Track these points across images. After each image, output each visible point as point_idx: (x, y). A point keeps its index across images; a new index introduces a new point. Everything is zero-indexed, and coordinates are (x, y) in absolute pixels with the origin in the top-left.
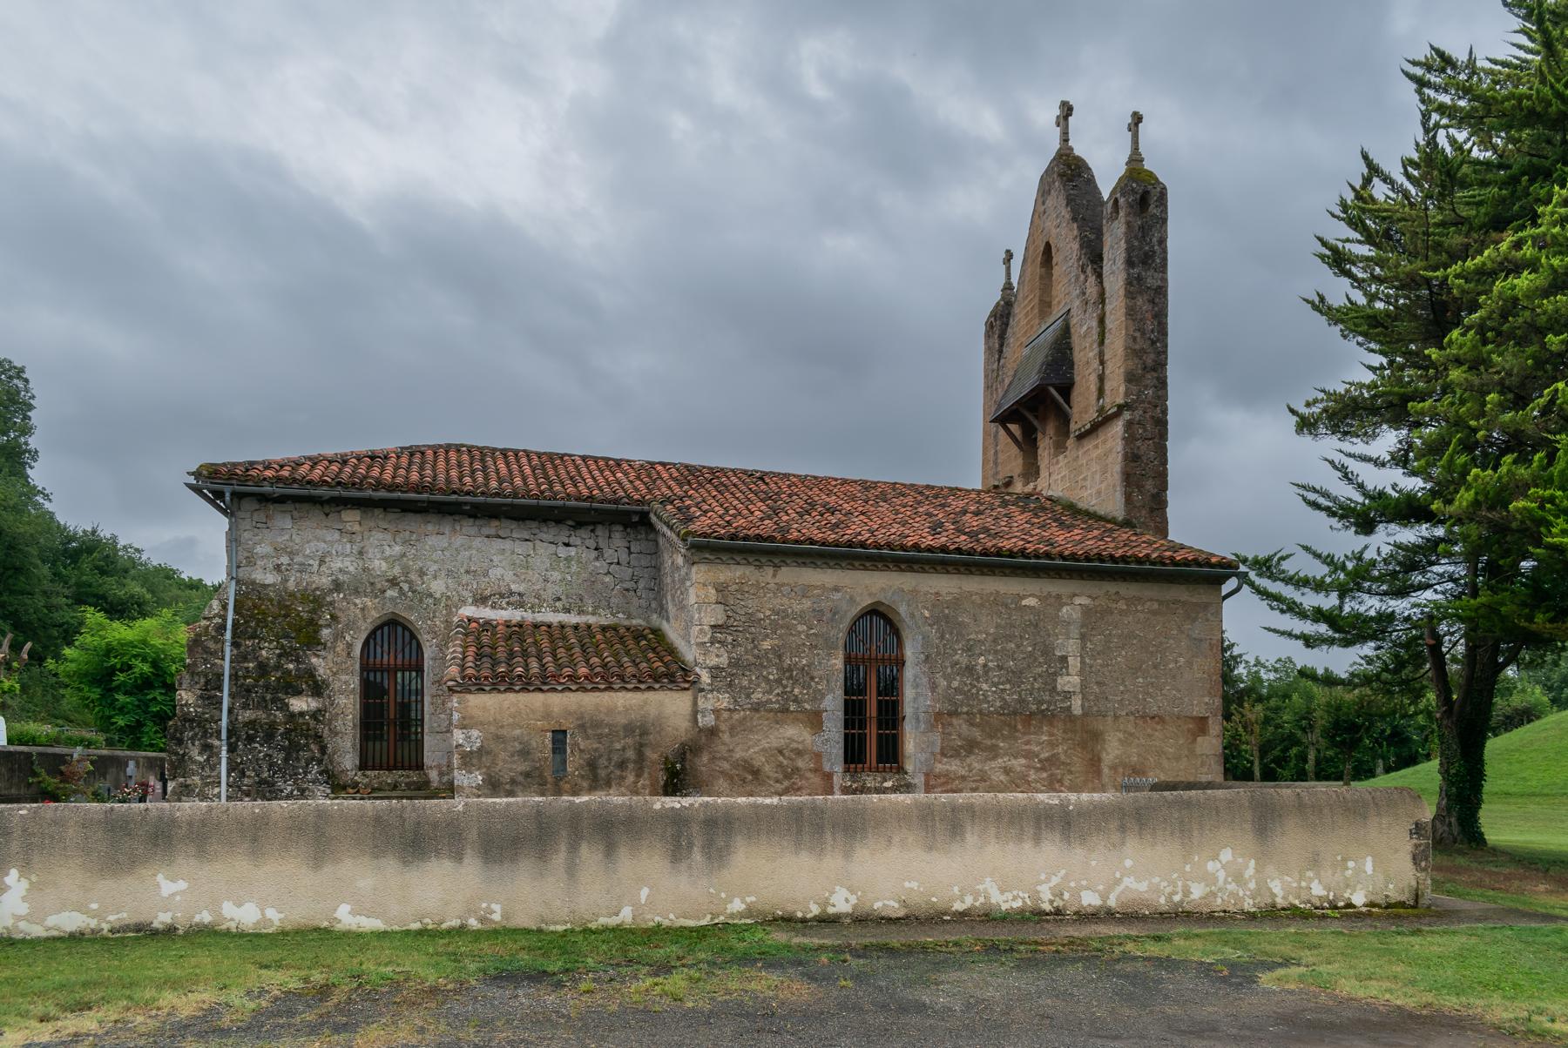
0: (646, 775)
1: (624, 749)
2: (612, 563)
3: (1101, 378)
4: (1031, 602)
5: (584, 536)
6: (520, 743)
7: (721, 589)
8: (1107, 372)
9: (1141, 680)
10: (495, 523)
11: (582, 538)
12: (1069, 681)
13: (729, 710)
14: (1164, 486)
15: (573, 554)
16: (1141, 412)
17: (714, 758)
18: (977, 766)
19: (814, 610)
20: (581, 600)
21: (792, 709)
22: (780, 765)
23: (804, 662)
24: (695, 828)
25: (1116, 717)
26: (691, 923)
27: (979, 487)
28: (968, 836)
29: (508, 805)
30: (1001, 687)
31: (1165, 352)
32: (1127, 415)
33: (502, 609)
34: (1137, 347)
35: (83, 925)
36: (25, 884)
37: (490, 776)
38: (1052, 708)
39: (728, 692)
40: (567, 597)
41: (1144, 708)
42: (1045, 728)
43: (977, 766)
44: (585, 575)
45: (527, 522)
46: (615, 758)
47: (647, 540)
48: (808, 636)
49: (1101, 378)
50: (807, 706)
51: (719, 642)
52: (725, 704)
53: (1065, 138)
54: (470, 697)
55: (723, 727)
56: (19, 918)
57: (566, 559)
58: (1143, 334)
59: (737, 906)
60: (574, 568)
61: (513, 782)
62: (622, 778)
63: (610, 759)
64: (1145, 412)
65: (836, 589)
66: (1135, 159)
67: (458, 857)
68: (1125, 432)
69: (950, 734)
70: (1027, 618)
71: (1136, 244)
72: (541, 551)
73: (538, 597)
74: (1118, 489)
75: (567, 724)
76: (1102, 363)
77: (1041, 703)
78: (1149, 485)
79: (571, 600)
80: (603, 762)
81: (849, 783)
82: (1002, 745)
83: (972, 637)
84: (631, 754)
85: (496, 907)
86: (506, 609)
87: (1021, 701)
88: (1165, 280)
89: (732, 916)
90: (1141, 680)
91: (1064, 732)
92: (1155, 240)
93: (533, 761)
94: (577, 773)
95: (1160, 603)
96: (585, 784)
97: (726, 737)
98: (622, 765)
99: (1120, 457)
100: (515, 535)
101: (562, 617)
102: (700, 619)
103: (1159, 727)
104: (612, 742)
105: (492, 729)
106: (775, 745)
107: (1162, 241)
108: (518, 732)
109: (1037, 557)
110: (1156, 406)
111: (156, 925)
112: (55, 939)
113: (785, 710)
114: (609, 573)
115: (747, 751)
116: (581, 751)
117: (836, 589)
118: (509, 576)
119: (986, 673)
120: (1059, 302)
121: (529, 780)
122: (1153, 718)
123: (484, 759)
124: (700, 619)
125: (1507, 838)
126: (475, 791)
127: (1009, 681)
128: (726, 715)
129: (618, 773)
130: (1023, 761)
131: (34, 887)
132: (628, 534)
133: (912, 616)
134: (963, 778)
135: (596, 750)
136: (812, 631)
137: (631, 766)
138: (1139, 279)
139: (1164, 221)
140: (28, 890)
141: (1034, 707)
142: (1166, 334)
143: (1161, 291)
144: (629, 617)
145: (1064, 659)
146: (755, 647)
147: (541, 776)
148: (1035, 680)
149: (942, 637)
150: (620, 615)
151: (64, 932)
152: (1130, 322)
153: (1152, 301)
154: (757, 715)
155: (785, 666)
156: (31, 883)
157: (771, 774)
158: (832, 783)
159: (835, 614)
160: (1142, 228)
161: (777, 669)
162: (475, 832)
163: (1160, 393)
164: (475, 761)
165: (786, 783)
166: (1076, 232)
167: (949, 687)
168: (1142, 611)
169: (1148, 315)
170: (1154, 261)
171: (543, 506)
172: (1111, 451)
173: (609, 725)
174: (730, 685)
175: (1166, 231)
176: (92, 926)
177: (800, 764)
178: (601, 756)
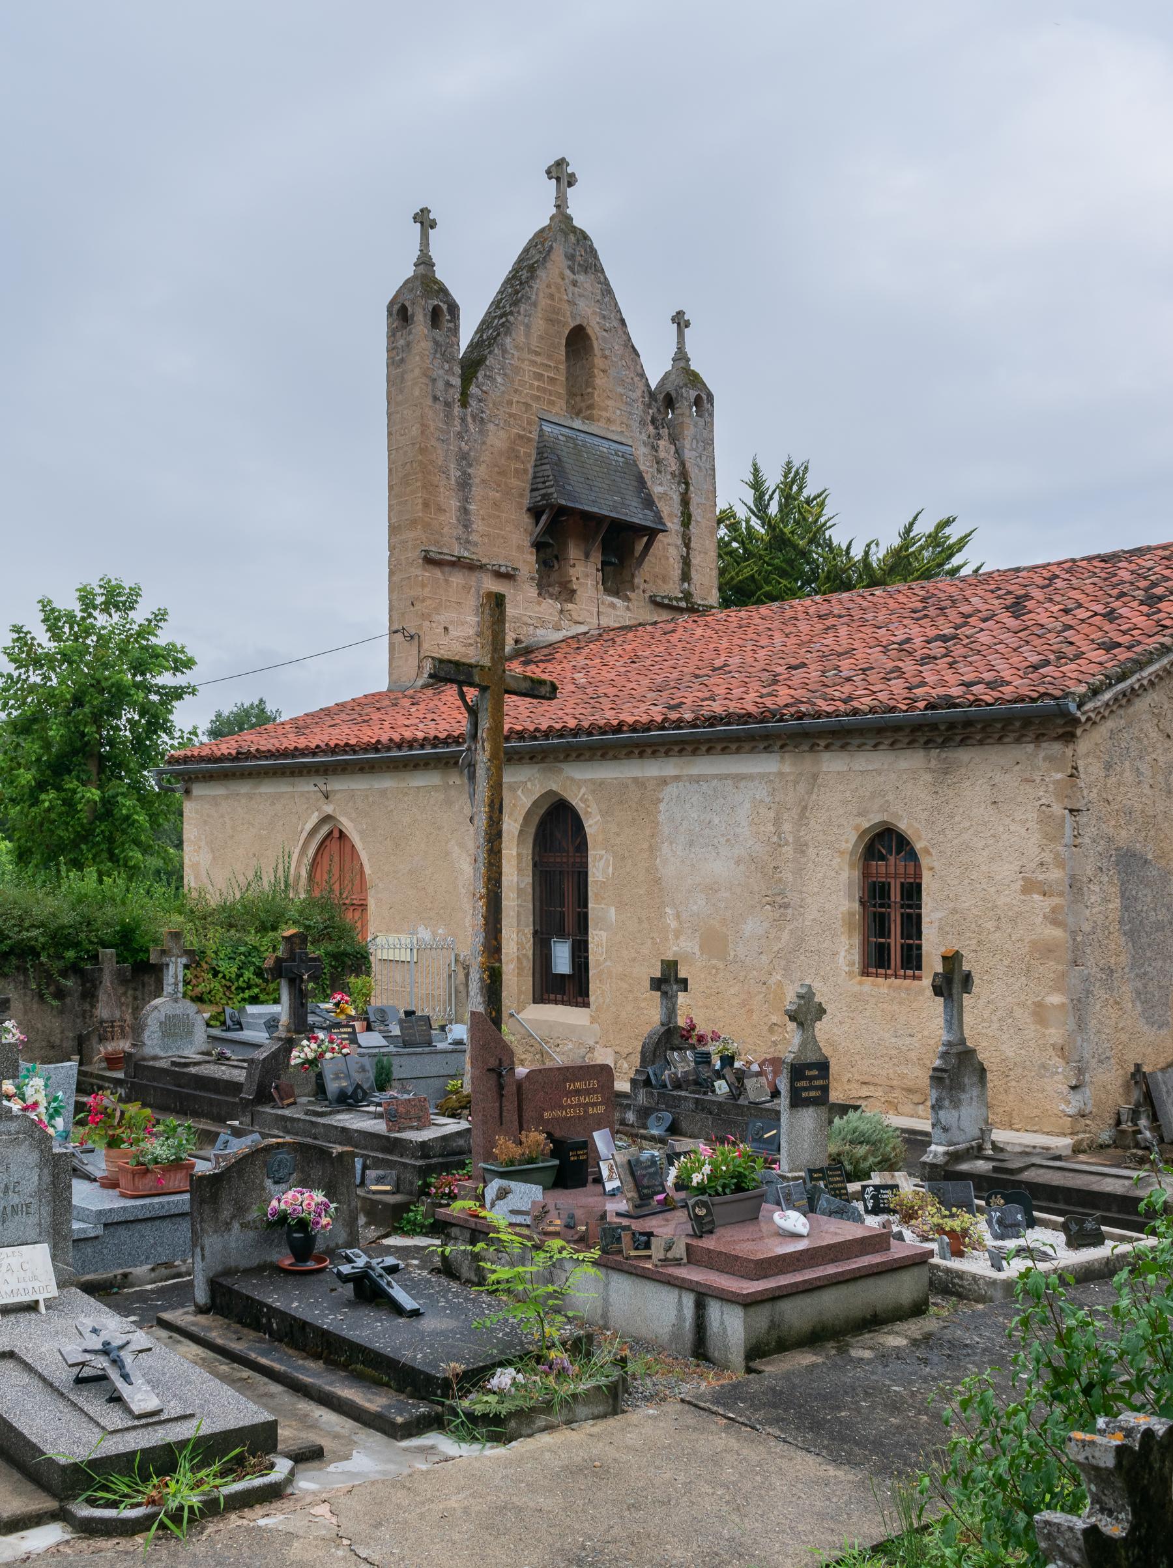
3: (686, 562)
49: (686, 562)
66: (425, 262)
76: (687, 545)
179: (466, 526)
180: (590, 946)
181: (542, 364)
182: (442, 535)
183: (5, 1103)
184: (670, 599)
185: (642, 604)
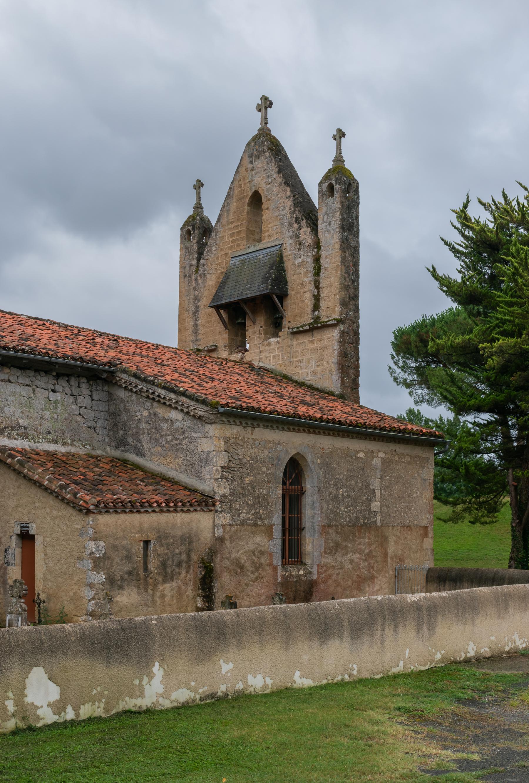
0: (191, 571)
1: (180, 553)
2: (81, 407)
3: (317, 298)
4: (361, 455)
5: (64, 385)
6: (126, 551)
7: (227, 441)
8: (322, 295)
9: (403, 504)
10: (7, 370)
11: (63, 387)
12: (376, 505)
13: (230, 525)
14: (357, 375)
15: (59, 398)
16: (348, 326)
17: (223, 558)
18: (339, 559)
19: (270, 457)
20: (63, 434)
21: (259, 524)
22: (253, 562)
23: (265, 492)
24: (425, 611)
25: (393, 527)
26: (423, 668)
27: (174, 344)
28: (510, 609)
29: (355, 603)
30: (349, 509)
31: (358, 289)
32: (342, 327)
33: (15, 439)
34: (346, 283)
35: (188, 697)
36: (162, 672)
37: (109, 576)
38: (369, 522)
39: (229, 513)
40: (55, 431)
41: (404, 521)
42: (367, 534)
43: (339, 559)
44: (66, 415)
45: (28, 371)
46: (176, 559)
47: (103, 390)
48: (267, 475)
49: (317, 298)
50: (266, 522)
51: (225, 478)
52: (228, 521)
53: (265, 120)
54: (100, 517)
55: (227, 537)
56: (158, 695)
57: (55, 402)
58: (349, 275)
59: (438, 657)
60: (59, 410)
61: (122, 579)
62: (179, 574)
63: (173, 561)
64: (349, 326)
65: (279, 444)
66: (339, 160)
67: (341, 638)
68: (341, 337)
69: (328, 539)
70: (359, 465)
71: (346, 217)
72: (38, 395)
73: (36, 430)
74: (335, 373)
75: (152, 536)
76: (317, 287)
77: (365, 518)
78: (351, 372)
79: (57, 434)
80: (170, 563)
81: (284, 573)
82: (349, 545)
83: (337, 476)
84: (184, 557)
85: (355, 666)
86: (17, 440)
87: (357, 517)
88: (358, 242)
89: (437, 662)
90: (403, 504)
91: (375, 537)
92: (354, 216)
93: (133, 563)
94: (156, 571)
95: (411, 457)
96: (160, 579)
97: (228, 543)
98: (179, 565)
99: (336, 353)
100: (20, 381)
101: (52, 447)
102: (216, 462)
103: (409, 533)
104: (174, 549)
105: (111, 540)
106: (251, 548)
107: (357, 217)
108: (125, 542)
109: (327, 422)
110: (354, 323)
111: (220, 694)
112: (177, 708)
113: (255, 525)
114: (80, 414)
115: (238, 552)
116: (159, 555)
117: (279, 444)
118: (18, 413)
119: (343, 499)
120: (270, 236)
121: (131, 577)
122: (407, 527)
123: (106, 563)
124: (216, 462)
125: (444, 594)
126: (101, 586)
127: (352, 505)
128: (228, 528)
129: (177, 570)
130: (358, 555)
131: (167, 674)
132: (92, 385)
133: (313, 462)
134: (333, 567)
135: (166, 554)
136: (269, 472)
137: (184, 565)
138: (347, 239)
139: (358, 204)
140: (163, 676)
141: (362, 521)
142: (358, 277)
143: (356, 249)
144: (93, 448)
145: (374, 490)
146: (242, 482)
147: (138, 575)
148: (363, 504)
149: (325, 477)
150: (88, 447)
151: (180, 703)
152: (343, 266)
153: (352, 255)
154: (243, 528)
155: (256, 495)
156: (165, 671)
157: (249, 568)
158: (277, 573)
159: (279, 460)
160: (348, 207)
161: (253, 497)
162: (347, 621)
163: (356, 314)
164: (101, 564)
165: (256, 574)
166: (289, 193)
167: (328, 508)
168: (404, 462)
169: (351, 264)
170: (353, 229)
171: (38, 360)
172: (327, 347)
173: (173, 537)
174: (230, 508)
175: (359, 211)
176: (192, 698)
177: (263, 561)
178: (169, 559)
179: (196, 333)
180: (511, 538)
181: (235, 227)
182: (186, 342)
183: (24, 582)
184: (298, 328)
185: (286, 336)
